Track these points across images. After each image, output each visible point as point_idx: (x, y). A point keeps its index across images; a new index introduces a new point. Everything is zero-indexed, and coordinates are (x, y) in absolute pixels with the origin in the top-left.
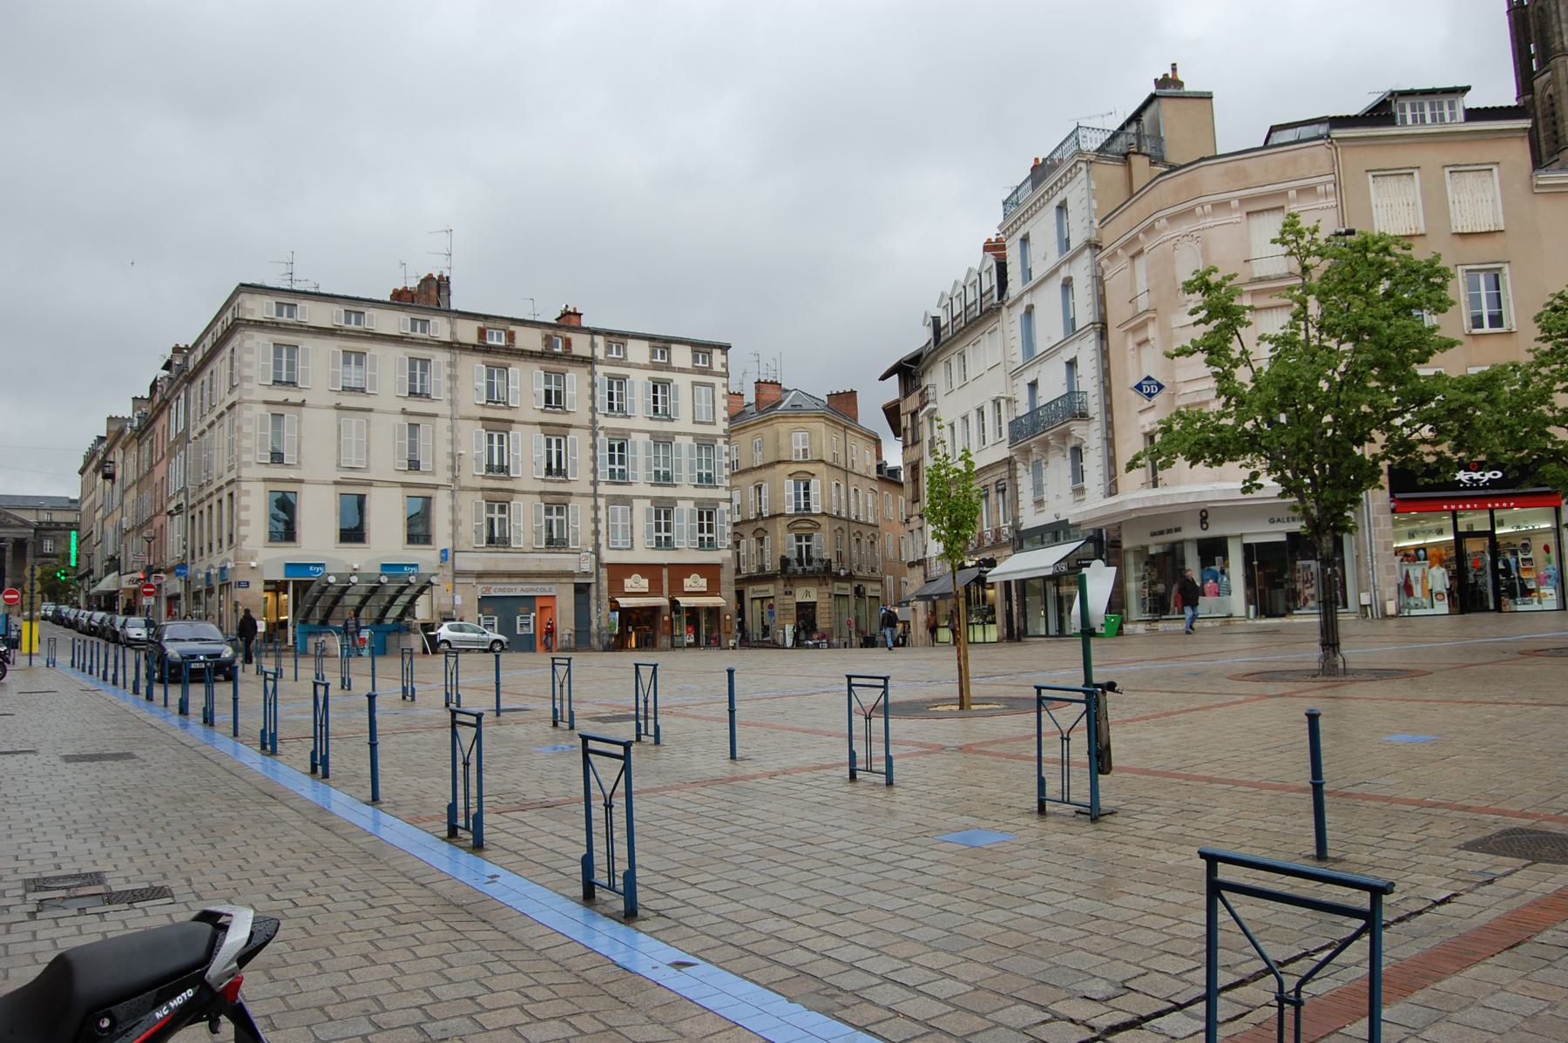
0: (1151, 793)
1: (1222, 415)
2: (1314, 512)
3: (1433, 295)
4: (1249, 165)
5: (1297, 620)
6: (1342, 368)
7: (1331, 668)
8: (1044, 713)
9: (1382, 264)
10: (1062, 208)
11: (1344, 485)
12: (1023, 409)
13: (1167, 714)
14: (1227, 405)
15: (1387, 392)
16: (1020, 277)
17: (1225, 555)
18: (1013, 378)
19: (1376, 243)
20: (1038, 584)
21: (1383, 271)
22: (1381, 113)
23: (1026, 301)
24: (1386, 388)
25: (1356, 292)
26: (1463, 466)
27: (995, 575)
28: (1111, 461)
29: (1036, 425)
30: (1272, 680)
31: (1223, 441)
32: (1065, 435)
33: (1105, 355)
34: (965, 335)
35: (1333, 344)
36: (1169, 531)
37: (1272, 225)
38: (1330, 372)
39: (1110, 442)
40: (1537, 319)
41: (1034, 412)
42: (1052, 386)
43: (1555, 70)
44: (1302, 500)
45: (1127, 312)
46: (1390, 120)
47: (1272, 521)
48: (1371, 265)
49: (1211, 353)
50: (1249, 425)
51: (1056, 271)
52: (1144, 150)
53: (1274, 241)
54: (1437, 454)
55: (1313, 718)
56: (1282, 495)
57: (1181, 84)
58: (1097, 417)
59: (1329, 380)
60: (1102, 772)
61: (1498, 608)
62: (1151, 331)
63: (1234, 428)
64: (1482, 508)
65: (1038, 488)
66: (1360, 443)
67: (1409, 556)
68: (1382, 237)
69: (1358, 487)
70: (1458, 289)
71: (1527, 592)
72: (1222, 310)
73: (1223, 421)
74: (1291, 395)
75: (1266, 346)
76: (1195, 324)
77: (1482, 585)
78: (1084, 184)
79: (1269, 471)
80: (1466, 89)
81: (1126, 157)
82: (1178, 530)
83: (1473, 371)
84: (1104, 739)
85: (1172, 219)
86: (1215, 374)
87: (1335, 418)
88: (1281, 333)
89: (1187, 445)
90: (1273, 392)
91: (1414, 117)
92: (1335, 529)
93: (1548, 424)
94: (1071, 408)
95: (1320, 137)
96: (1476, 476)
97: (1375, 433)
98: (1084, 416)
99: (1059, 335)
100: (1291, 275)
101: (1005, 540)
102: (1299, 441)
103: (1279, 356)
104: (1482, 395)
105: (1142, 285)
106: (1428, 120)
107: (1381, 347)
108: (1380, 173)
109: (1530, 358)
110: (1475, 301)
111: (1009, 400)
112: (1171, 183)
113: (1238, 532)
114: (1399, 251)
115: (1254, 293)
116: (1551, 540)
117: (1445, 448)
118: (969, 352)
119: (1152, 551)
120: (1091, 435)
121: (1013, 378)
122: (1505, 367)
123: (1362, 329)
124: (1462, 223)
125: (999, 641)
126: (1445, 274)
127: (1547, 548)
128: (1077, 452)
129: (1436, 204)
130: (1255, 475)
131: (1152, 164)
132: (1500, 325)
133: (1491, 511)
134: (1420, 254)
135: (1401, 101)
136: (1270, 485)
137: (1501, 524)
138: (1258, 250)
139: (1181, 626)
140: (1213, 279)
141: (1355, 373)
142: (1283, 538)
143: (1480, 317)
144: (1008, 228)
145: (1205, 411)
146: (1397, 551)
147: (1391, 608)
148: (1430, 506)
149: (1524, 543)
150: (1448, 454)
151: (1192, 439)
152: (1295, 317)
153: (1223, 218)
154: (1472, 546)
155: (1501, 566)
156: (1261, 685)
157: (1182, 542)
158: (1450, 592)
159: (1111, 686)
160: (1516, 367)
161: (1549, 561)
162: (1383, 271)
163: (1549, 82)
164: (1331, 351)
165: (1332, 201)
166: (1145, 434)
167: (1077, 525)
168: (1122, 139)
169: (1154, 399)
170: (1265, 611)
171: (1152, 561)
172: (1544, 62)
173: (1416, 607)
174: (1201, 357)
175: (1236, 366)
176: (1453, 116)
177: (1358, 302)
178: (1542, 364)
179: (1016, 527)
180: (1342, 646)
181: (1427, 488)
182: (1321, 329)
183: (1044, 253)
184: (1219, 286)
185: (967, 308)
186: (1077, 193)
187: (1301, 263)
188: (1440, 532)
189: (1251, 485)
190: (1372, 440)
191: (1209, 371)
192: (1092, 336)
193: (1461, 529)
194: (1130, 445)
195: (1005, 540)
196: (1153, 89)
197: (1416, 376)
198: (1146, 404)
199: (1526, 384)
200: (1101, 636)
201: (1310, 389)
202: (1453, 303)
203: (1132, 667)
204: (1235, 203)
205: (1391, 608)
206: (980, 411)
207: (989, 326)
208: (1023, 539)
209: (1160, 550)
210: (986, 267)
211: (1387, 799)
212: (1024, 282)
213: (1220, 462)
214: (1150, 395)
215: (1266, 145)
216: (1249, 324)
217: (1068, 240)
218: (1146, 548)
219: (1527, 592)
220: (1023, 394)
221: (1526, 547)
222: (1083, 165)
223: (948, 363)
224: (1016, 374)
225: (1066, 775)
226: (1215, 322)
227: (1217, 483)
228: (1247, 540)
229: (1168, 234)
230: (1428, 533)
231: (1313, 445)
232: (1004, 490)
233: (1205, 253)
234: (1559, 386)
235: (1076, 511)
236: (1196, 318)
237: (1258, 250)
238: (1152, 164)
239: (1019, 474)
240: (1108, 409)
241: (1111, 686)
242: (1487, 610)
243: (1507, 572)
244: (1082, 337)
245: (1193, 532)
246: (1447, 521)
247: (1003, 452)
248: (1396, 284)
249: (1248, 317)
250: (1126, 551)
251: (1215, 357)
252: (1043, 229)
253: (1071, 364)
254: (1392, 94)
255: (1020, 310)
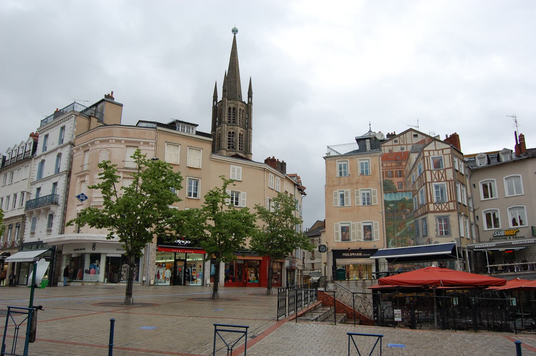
0: (52, 350)
1: (104, 211)
2: (130, 248)
3: (177, 184)
4: (130, 130)
5: (121, 285)
6: (146, 202)
7: (128, 302)
8: (10, 317)
9: (163, 171)
10: (63, 128)
11: (141, 240)
12: (33, 197)
13: (65, 318)
14: (106, 208)
15: (159, 212)
16: (42, 149)
17: (100, 260)
18: (31, 185)
19: (162, 164)
20: (27, 264)
21: (162, 174)
22: (173, 125)
23: (42, 158)
24: (159, 210)
25: (154, 178)
26: (178, 238)
27: (10, 259)
28: (64, 221)
29: (37, 204)
30: (107, 306)
31: (103, 220)
32: (48, 209)
33: (68, 183)
34: (15, 166)
35: (144, 193)
36: (81, 249)
37: (132, 151)
38: (142, 203)
39: (64, 214)
40: (205, 197)
41: (37, 199)
42: (46, 190)
43: (222, 127)
44: (126, 244)
45: (80, 169)
46: (175, 128)
47: (117, 250)
48: (160, 171)
49: (104, 190)
50: (113, 216)
51: (56, 150)
52: (96, 116)
53: (131, 157)
54: (171, 234)
55: (112, 322)
56: (120, 241)
57: (114, 99)
58: (61, 205)
59: (141, 205)
60: (30, 342)
61: (184, 284)
62: (87, 178)
63: (108, 216)
64: (183, 252)
65: (33, 228)
66: (148, 227)
67: (159, 265)
68: (165, 163)
69: (145, 241)
70: (185, 184)
71: (193, 280)
72: (110, 176)
73: (104, 213)
74: (128, 208)
75: (124, 190)
76: (100, 178)
77: (180, 277)
78: (73, 122)
79: (117, 232)
80: (197, 125)
81: (90, 117)
82: (84, 249)
83: (186, 209)
84: (34, 328)
85: (101, 142)
86: (104, 197)
87: (141, 218)
88: (129, 187)
89: (90, 220)
90: (122, 207)
91: (182, 129)
92: (136, 255)
93: (204, 229)
94: (52, 200)
95: (153, 128)
96: (183, 242)
97: (153, 225)
98: (56, 204)
99: (52, 172)
100: (136, 169)
101: (16, 246)
102: (128, 224)
103: (127, 194)
104: (186, 217)
105: (86, 161)
106: (186, 131)
107: (159, 197)
108: (169, 144)
109: (202, 208)
110: (190, 188)
111: (28, 193)
112: (103, 130)
113: (105, 252)
114: (169, 168)
115: (124, 172)
116: (202, 264)
117: (174, 232)
118: (16, 172)
119: (73, 256)
120: (58, 211)
121: (31, 185)
122: (194, 210)
123: (154, 190)
124: (190, 164)
125: (6, 286)
126: (181, 178)
127: (200, 266)
128: (51, 217)
129: (183, 157)
130: (112, 233)
131: (98, 122)
132: (196, 197)
133: (186, 253)
134: (175, 170)
135: (179, 123)
136: (116, 237)
137: (189, 258)
138: (124, 158)
139: (79, 284)
140: (108, 165)
141: (149, 204)
142: (120, 256)
143: (191, 193)
144: (41, 130)
145: (99, 209)
146: (157, 264)
147: (152, 282)
148: (169, 250)
149: (194, 264)
150: (174, 234)
151: (93, 218)
152: (134, 183)
153: (118, 145)
154: (180, 264)
155: (187, 271)
156: (103, 308)
157: (85, 253)
158: (171, 278)
159: (40, 308)
160: (197, 210)
161: (200, 270)
162: (162, 174)
163: (220, 129)
164: (144, 196)
165: (153, 148)
166: (78, 214)
167: (46, 243)
168: (90, 111)
169: (83, 202)
170: (111, 281)
171: (72, 259)
172: (220, 124)
173: (160, 282)
174: (100, 190)
175: (112, 195)
176: (192, 132)
177: (154, 182)
178: (205, 210)
179: (21, 242)
180: (133, 294)
181: (166, 244)
182: (142, 188)
183: (53, 142)
184: (110, 167)
185: (18, 155)
186: (69, 125)
187: (139, 166)
188: (171, 258)
189: (110, 236)
190: (152, 227)
191: (102, 195)
192: (65, 175)
193: (177, 258)
194: (72, 215)
195: (16, 246)
196: (104, 98)
197: (168, 208)
198: (80, 203)
199: (200, 216)
200: (39, 288)
201: (134, 207)
202: (182, 188)
203: (57, 299)
204: (123, 142)
205: (152, 282)
206: (15, 195)
207: (26, 164)
208: (23, 246)
209: (76, 255)
210: (29, 142)
211: (136, 350)
212: (43, 151)
213: (101, 227)
214: (82, 200)
215: (137, 126)
216: (118, 182)
217: (63, 140)
218: (71, 255)
219: (193, 280)
220: (34, 192)
221: (195, 266)
222: (74, 116)
223: (6, 175)
224: (33, 184)
225: (15, 343)
226: (107, 179)
227: (98, 234)
228: (108, 255)
229: (98, 146)
230: (166, 259)
231: (133, 226)
232: (19, 227)
233: (110, 155)
234: (208, 218)
235: (47, 238)
236: (101, 176)
237: (124, 158)
238: (98, 122)
239: (27, 221)
240: (66, 202)
241: (40, 308)
242: (181, 284)
243: (188, 273)
244: (61, 175)
245: (89, 250)
246: (173, 255)
247: (22, 212)
248: (166, 178)
249: (118, 179)
250: (64, 255)
251: (105, 191)
252: (54, 134)
253: (55, 184)
254: (177, 121)
255: (39, 161)
